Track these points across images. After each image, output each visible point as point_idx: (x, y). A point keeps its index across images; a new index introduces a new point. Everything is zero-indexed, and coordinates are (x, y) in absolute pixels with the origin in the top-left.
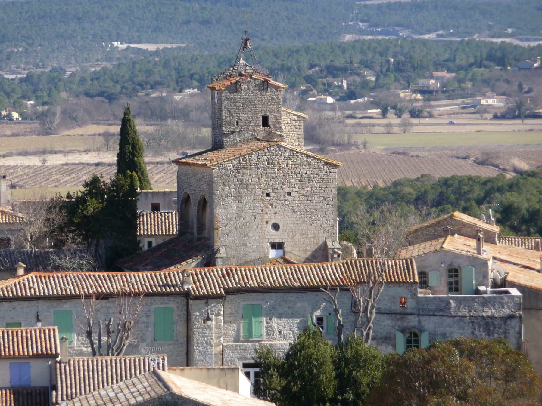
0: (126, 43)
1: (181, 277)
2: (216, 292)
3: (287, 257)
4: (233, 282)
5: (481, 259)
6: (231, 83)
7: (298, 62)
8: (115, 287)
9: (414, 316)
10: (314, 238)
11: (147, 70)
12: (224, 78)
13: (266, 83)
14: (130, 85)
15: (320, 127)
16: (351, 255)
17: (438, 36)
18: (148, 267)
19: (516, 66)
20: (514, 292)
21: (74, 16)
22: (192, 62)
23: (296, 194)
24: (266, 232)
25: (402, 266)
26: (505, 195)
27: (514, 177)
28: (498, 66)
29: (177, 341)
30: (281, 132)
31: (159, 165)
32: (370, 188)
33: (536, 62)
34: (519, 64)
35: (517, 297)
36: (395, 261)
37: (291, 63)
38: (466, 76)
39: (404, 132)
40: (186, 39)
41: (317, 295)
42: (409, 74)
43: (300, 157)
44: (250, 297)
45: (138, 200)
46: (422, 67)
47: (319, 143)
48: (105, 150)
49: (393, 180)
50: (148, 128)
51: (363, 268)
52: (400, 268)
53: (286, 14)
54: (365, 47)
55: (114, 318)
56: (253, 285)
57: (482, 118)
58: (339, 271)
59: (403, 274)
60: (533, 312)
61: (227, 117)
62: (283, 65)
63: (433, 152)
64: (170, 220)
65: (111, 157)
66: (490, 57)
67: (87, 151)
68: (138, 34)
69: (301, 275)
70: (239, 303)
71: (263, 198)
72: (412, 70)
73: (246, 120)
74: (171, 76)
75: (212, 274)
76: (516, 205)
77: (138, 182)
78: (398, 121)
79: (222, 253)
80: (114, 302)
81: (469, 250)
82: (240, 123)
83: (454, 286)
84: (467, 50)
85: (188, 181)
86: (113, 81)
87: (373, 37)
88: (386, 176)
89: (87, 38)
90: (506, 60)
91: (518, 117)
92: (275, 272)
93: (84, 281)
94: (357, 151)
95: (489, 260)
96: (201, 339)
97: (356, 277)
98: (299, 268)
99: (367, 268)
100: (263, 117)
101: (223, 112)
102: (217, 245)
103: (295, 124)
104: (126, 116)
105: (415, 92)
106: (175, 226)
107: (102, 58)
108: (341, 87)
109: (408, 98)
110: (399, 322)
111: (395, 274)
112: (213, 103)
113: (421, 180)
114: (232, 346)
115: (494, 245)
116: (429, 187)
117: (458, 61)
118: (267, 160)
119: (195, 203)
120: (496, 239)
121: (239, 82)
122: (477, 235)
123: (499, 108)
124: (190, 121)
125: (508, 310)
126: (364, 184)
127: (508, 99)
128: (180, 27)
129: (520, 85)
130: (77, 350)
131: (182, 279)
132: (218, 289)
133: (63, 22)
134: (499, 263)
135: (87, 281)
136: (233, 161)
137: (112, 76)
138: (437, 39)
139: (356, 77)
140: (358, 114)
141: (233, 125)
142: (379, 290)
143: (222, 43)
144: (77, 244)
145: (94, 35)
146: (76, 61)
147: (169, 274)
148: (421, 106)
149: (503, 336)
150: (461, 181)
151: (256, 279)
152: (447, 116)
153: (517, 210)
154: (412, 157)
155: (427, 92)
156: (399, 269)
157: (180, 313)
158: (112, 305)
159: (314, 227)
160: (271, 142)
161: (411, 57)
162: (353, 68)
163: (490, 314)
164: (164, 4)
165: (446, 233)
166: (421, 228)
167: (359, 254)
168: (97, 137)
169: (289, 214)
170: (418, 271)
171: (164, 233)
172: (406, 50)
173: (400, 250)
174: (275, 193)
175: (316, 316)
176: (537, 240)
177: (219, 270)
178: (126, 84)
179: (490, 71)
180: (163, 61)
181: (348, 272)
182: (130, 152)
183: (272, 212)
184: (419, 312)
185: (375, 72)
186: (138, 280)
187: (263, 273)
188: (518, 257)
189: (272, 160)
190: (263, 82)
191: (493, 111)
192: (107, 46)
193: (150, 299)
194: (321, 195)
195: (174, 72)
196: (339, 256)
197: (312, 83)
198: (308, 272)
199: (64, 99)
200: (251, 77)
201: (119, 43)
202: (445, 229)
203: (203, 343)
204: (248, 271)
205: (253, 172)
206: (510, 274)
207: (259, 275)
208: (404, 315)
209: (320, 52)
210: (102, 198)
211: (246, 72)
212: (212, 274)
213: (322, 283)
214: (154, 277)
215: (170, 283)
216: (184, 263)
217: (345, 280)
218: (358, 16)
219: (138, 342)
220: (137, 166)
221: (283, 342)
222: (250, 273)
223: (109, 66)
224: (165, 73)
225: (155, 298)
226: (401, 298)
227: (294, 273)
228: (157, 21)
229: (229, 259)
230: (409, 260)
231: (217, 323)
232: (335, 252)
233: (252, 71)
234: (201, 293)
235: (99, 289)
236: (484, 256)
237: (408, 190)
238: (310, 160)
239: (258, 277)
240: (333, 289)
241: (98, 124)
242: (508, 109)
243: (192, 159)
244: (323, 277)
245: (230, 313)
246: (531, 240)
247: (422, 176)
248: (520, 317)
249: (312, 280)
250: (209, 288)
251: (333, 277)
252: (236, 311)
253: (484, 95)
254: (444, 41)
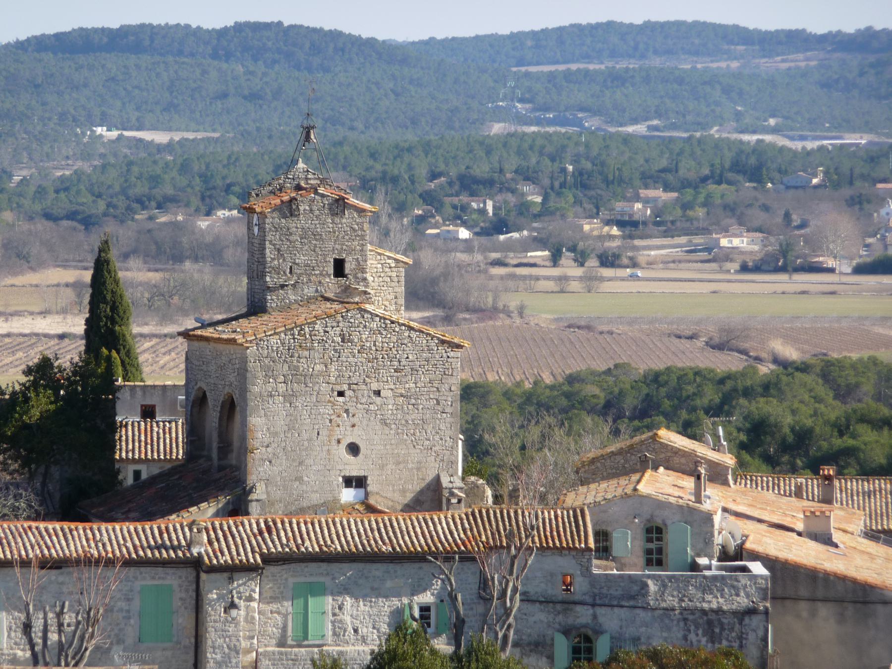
0: (118, 129)
1: (188, 534)
2: (248, 560)
3: (372, 501)
4: (277, 543)
5: (701, 512)
6: (282, 201)
7: (410, 167)
8: (73, 548)
9: (586, 607)
10: (418, 469)
11: (151, 177)
12: (271, 192)
13: (341, 202)
14: (121, 202)
15: (446, 280)
16: (482, 500)
17: (650, 128)
18: (132, 515)
19: (782, 183)
20: (757, 568)
21: (28, 80)
22: (229, 164)
23: (389, 394)
24: (336, 459)
25: (566, 520)
26: (757, 402)
27: (772, 371)
28: (750, 181)
29: (178, 643)
30: (367, 286)
31: (168, 340)
32: (528, 386)
33: (816, 177)
34: (785, 180)
35: (761, 577)
36: (555, 513)
37: (398, 168)
38: (695, 198)
39: (589, 292)
40: (221, 124)
41: (420, 568)
42: (599, 192)
43: (397, 329)
44: (306, 569)
45: (118, 398)
46: (621, 181)
47: (444, 307)
48: (76, 312)
49: (567, 372)
50: (151, 275)
51: (500, 523)
52: (564, 523)
53: (391, 85)
54: (526, 146)
55: (70, 602)
56: (310, 549)
57: (721, 271)
58: (460, 527)
59: (568, 533)
60: (788, 603)
61: (273, 259)
62: (384, 173)
63: (637, 327)
64: (174, 435)
65: (77, 325)
66: (738, 167)
67: (44, 313)
68: (137, 114)
69: (394, 533)
70: (286, 579)
71: (332, 399)
72: (603, 186)
73: (307, 265)
74: (192, 188)
75: (241, 528)
76: (772, 419)
77: (120, 368)
78: (579, 272)
79: (260, 493)
80: (70, 573)
81: (682, 495)
82: (297, 270)
83: (654, 556)
84: (699, 152)
85: (204, 367)
86: (93, 195)
87: (540, 129)
88: (556, 365)
89: (50, 119)
90: (764, 172)
91: (783, 269)
92: (349, 527)
93: (21, 536)
94: (508, 322)
95: (716, 512)
96: (220, 641)
97: (487, 538)
98: (390, 520)
99: (507, 524)
100: (336, 260)
101: (267, 251)
102: (251, 479)
103: (390, 274)
104: (103, 255)
105: (608, 223)
106: (181, 444)
107: (74, 154)
108: (483, 212)
109: (595, 233)
110: (561, 616)
111: (555, 533)
112: (251, 236)
113: (614, 373)
114: (274, 653)
115: (726, 488)
116: (628, 386)
117: (681, 172)
118: (340, 335)
119: (214, 406)
120: (730, 477)
121: (296, 200)
122: (696, 470)
123: (751, 253)
124: (221, 265)
125: (746, 600)
126: (518, 378)
127: (767, 238)
128: (211, 103)
129: (787, 216)
130: (9, 655)
131: (188, 538)
132: (250, 555)
133: (10, 91)
134: (732, 518)
135: (24, 536)
136: (283, 335)
137: (92, 185)
138: (648, 133)
139: (510, 195)
140: (512, 258)
141: (284, 272)
142: (527, 561)
143: (283, 132)
144: (11, 474)
145: (62, 116)
146: (31, 159)
147: (167, 529)
148: (618, 247)
149: (736, 645)
150: (682, 377)
151: (317, 539)
152: (661, 266)
153: (774, 429)
154: (601, 333)
155: (629, 225)
156: (561, 525)
157: (183, 595)
158: (68, 579)
159: (418, 451)
160: (348, 303)
161: (603, 164)
162: (504, 180)
163: (714, 606)
164: (183, 63)
165: (643, 465)
166: (602, 455)
167: (497, 499)
168: (62, 289)
169: (377, 427)
170: (593, 529)
171: (162, 457)
172: (595, 152)
173: (565, 492)
174: (354, 391)
175: (418, 604)
176: (799, 480)
177: (253, 522)
178: (115, 200)
179: (737, 191)
180: (180, 161)
181: (475, 529)
182: (107, 317)
183: (347, 423)
184: (595, 600)
185: (542, 187)
186: (113, 537)
187: (329, 529)
188: (766, 510)
189: (350, 335)
190: (337, 201)
191: (739, 259)
192: (84, 134)
193: (132, 571)
194: (432, 396)
195: (197, 179)
196: (459, 501)
197: (435, 204)
198: (407, 528)
199: (8, 224)
200: (316, 192)
201: (105, 128)
202: (643, 458)
203: (223, 647)
204: (302, 525)
205: (316, 355)
206: (751, 538)
207: (322, 531)
208: (568, 604)
209: (448, 152)
210: (56, 394)
211: (308, 184)
212: (241, 528)
213: (429, 548)
214: (141, 533)
215: (168, 543)
216: (193, 509)
217: (470, 542)
218: (514, 93)
219: (112, 643)
220: (119, 341)
221: (361, 648)
222: (307, 529)
223: (85, 166)
224: (183, 181)
225: (142, 569)
226: (565, 576)
227: (383, 530)
228: (171, 93)
229: (273, 504)
230: (578, 511)
231: (247, 614)
232: (452, 494)
233: (319, 182)
234: (222, 562)
235: (46, 552)
236: (706, 506)
237: (591, 390)
238: (414, 335)
239: (320, 536)
240: (448, 557)
241: (65, 267)
242: (766, 255)
243: (211, 330)
244: (432, 537)
245: (271, 597)
246: (790, 481)
247: (616, 366)
248: (766, 612)
249: (412, 542)
250: (235, 553)
251: (449, 537)
252: (282, 593)
253: (725, 231)
254: (659, 137)
